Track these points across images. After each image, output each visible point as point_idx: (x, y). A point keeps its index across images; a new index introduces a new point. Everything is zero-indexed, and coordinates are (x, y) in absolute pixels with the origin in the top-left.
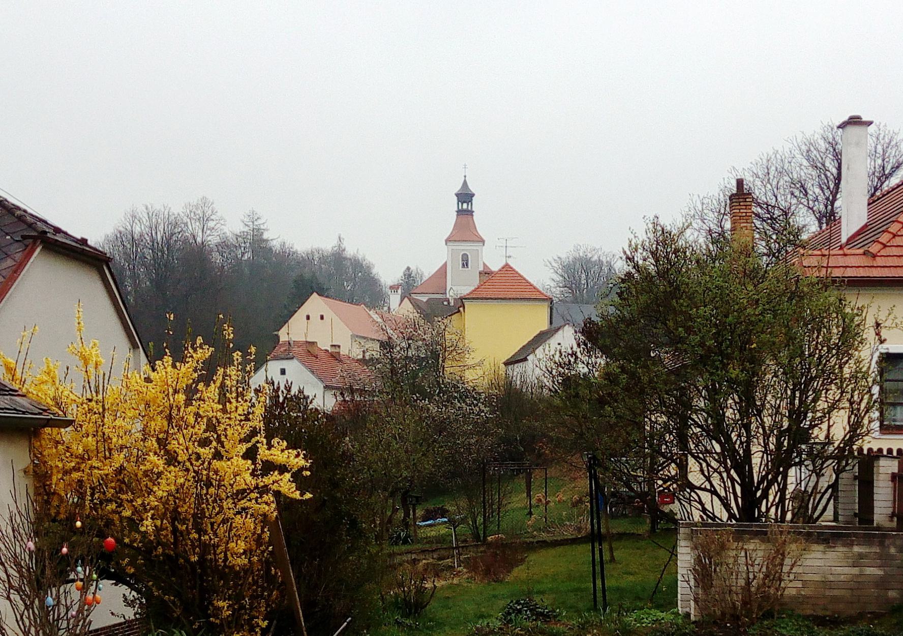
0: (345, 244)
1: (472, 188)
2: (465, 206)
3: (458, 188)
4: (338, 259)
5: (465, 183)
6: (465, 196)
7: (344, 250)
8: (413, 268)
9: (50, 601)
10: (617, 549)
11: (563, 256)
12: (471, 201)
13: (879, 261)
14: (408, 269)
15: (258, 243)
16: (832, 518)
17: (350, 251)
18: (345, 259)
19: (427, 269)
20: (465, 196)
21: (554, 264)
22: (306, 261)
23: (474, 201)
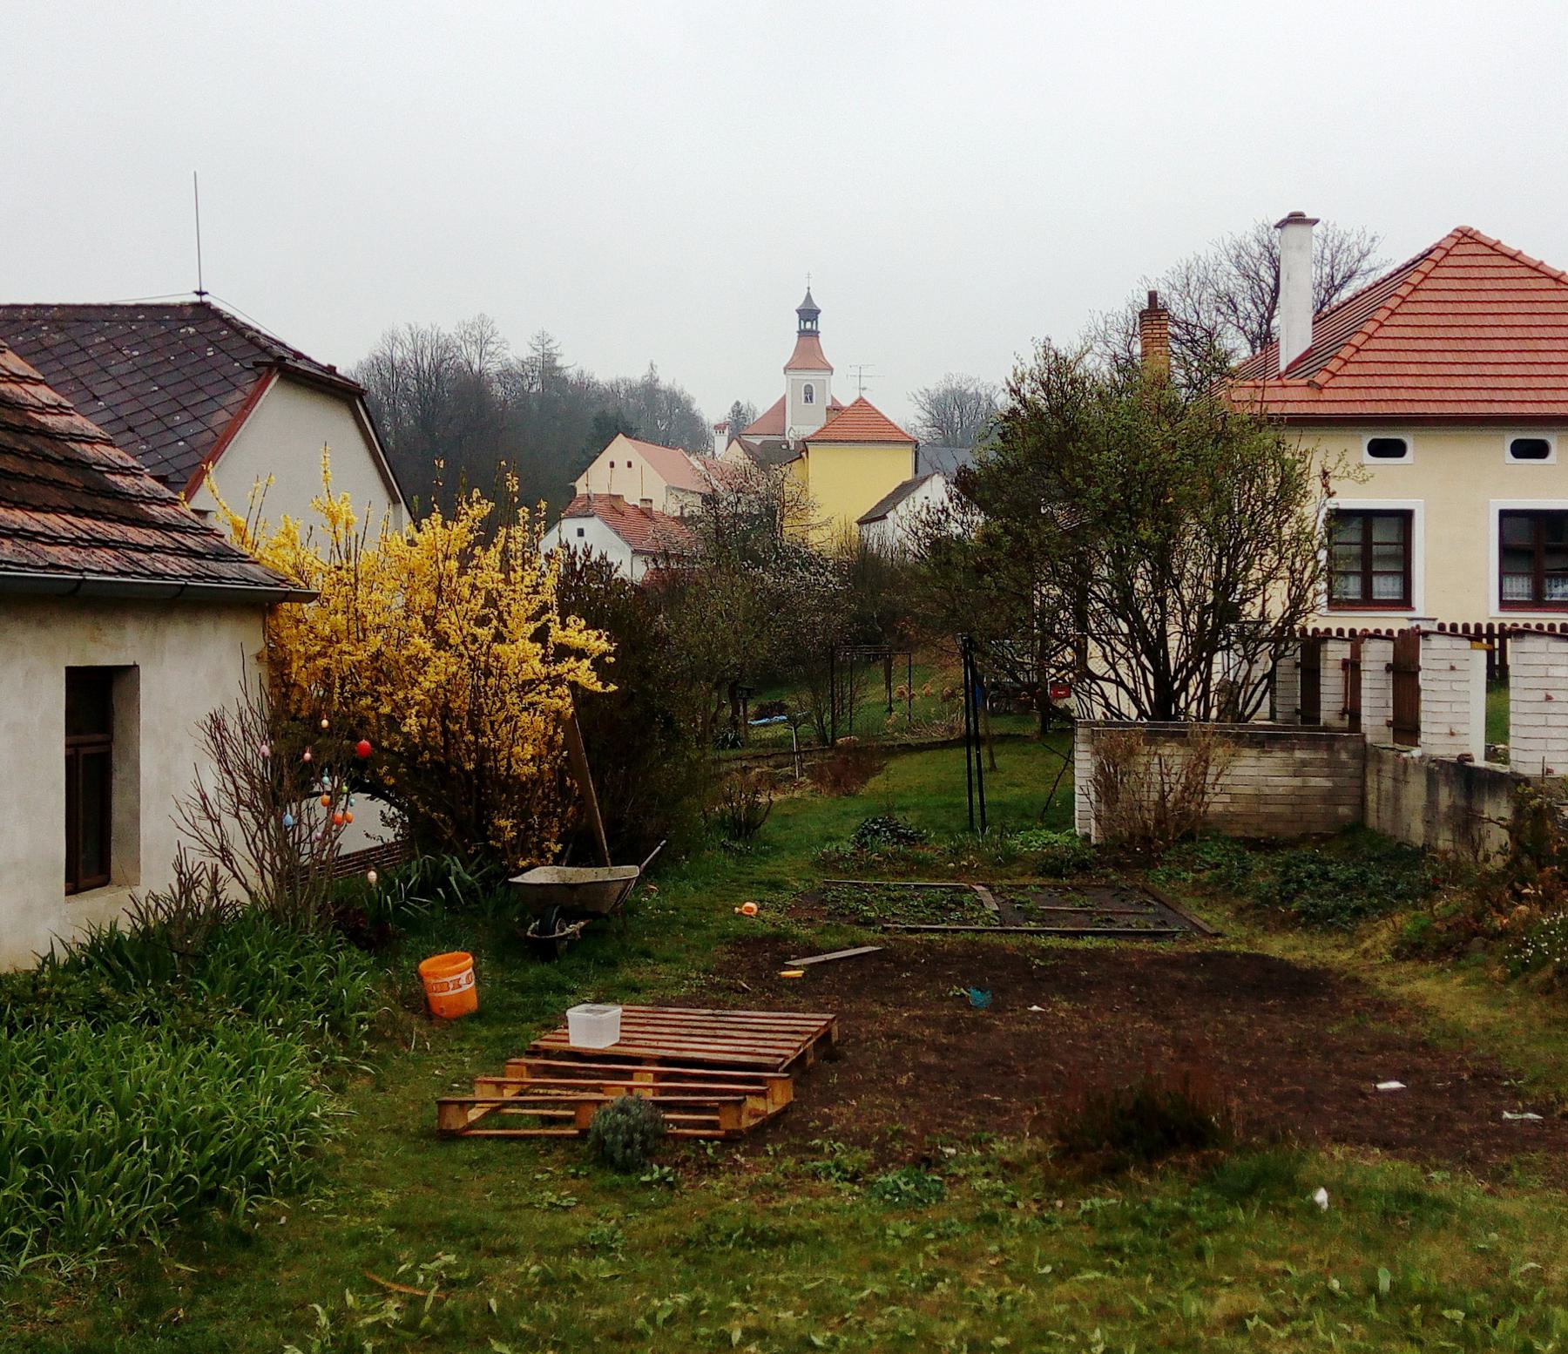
0: (659, 373)
1: (818, 302)
2: (808, 325)
5: (809, 296)
6: (809, 313)
8: (743, 403)
11: (932, 388)
14: (738, 403)
17: (665, 382)
18: (659, 391)
19: (761, 405)
20: (809, 313)
22: (609, 394)
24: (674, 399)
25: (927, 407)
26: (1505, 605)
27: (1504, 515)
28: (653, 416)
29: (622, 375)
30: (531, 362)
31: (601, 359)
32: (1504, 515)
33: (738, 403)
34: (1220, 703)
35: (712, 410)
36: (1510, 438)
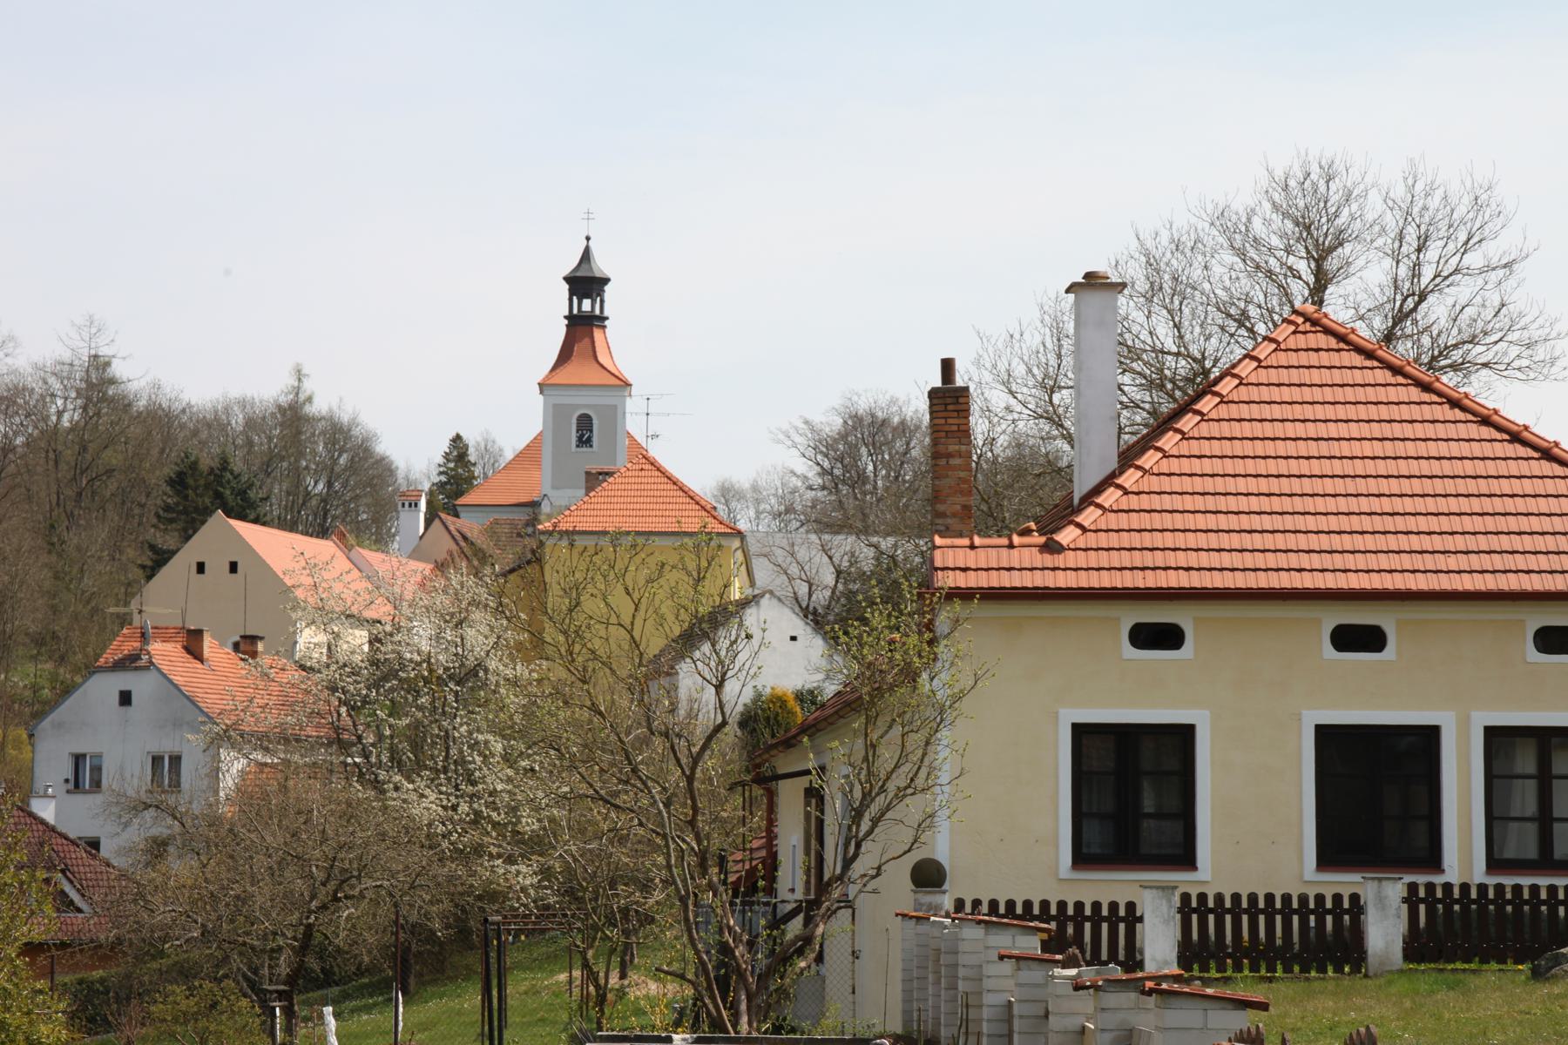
0: (308, 386)
1: (602, 264)
2: (587, 305)
3: (570, 263)
4: (292, 417)
5: (586, 256)
6: (585, 283)
7: (309, 399)
8: (471, 438)
9: (887, 756)
10: (518, 966)
11: (818, 418)
12: (600, 293)
13: (1059, 561)
14: (457, 439)
15: (97, 385)
16: (1532, 852)
17: (323, 401)
18: (310, 420)
19: (1239, 205)
20: (585, 283)
21: (798, 439)
22: (213, 424)
23: (607, 296)
24: (338, 433)
25: (810, 453)
26: (1495, 864)
27: (1081, 732)
28: (300, 470)
29: (235, 392)
30: (62, 371)
31: (199, 363)
32: (1081, 732)
33: (457, 439)
34: (75, 968)
35: (416, 458)
36: (1132, 615)
